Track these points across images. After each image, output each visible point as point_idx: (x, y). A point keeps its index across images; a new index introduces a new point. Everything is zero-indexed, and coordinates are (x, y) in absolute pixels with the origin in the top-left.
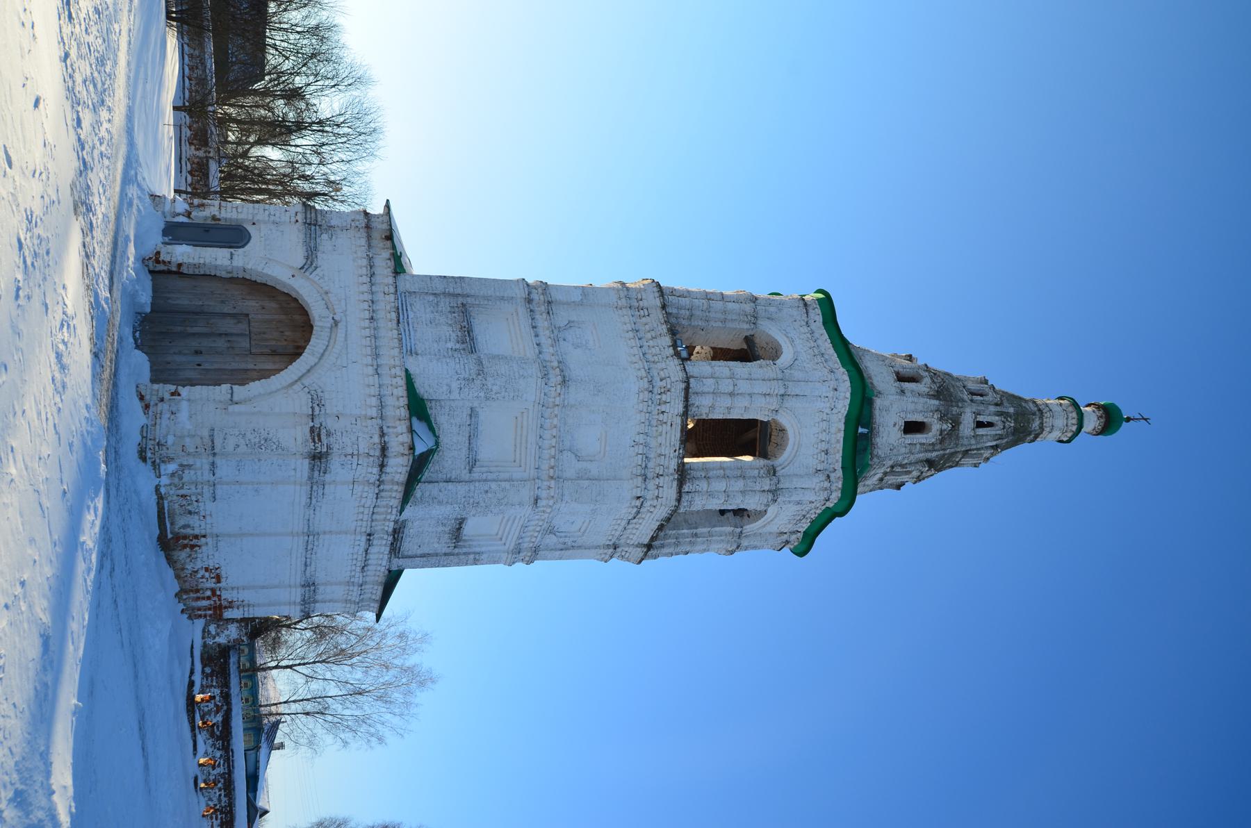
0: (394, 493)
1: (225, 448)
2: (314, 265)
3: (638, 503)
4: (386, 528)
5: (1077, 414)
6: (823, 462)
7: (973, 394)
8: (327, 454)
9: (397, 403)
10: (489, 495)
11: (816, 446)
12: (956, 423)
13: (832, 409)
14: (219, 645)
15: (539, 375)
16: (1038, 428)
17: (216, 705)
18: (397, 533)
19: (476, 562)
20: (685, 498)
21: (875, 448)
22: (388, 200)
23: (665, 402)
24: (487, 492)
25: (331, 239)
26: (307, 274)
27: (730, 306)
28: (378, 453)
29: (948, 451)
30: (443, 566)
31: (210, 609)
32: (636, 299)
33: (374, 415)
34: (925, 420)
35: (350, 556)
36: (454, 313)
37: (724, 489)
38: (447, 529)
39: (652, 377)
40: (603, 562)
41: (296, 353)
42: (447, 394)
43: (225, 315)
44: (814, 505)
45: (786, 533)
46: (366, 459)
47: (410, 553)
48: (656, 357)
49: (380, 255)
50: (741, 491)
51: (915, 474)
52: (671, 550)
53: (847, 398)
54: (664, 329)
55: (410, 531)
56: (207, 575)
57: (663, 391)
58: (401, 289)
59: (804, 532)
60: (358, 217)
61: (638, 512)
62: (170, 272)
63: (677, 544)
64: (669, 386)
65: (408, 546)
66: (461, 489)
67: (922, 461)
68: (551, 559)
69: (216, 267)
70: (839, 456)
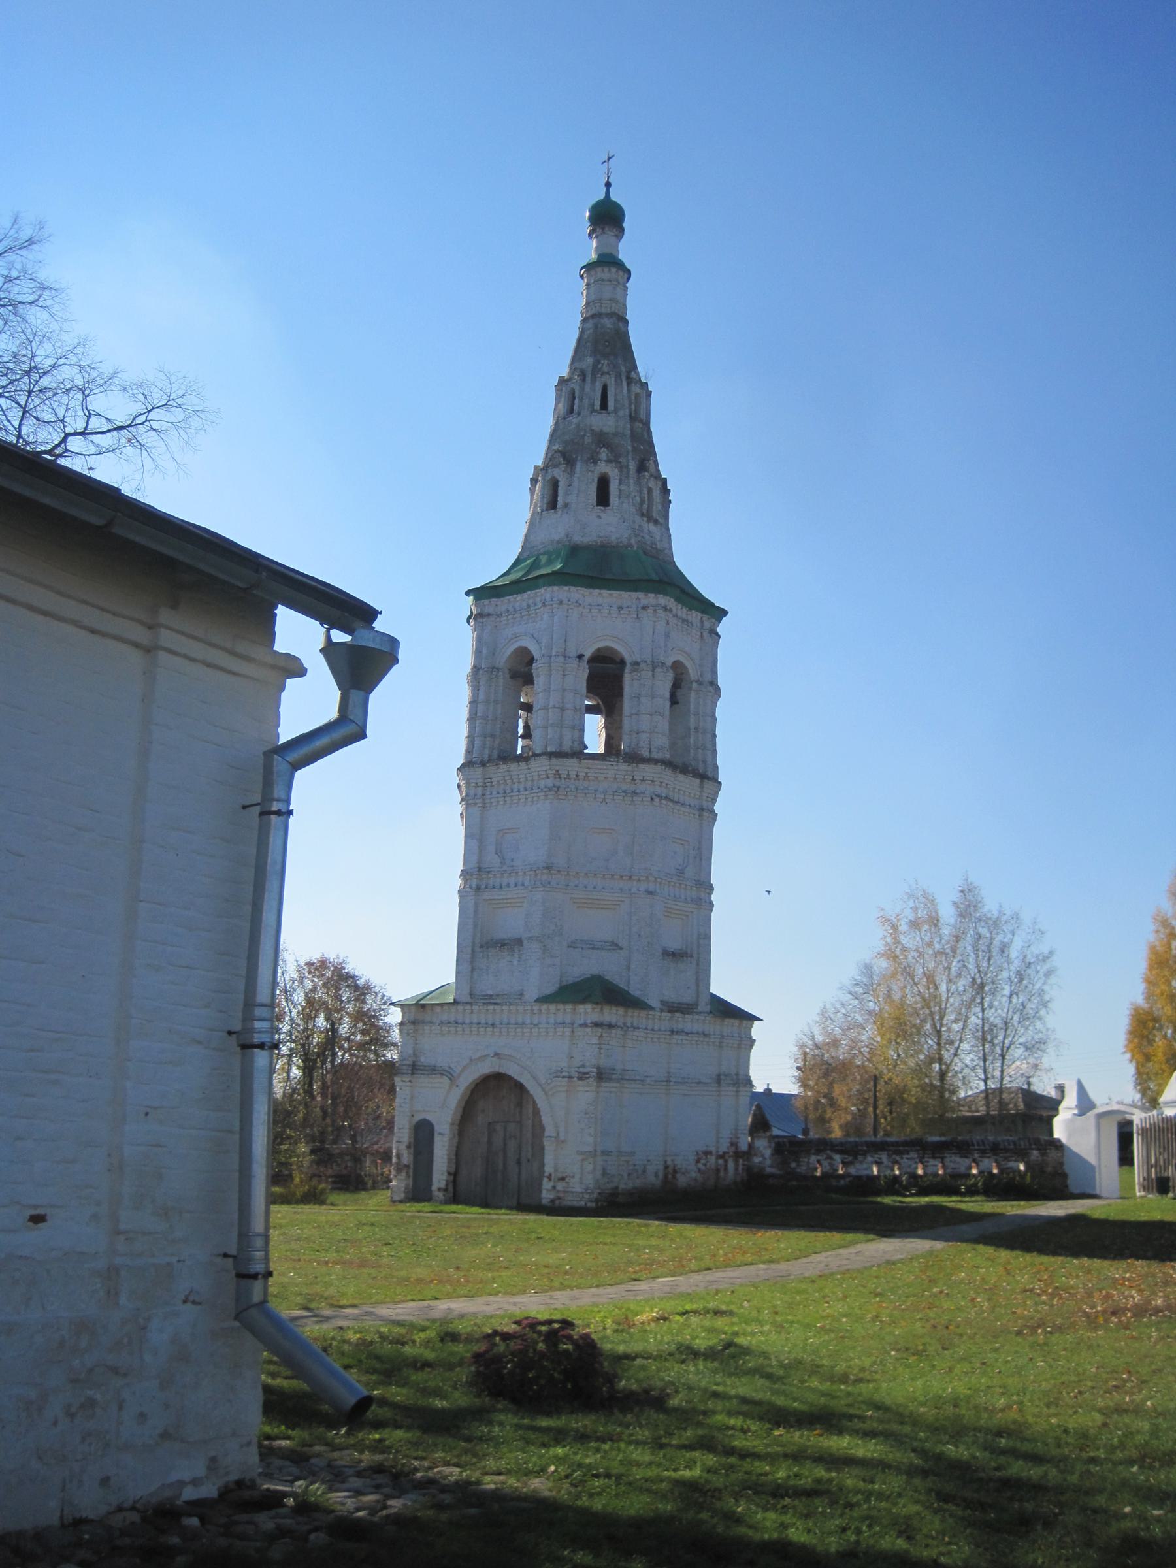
0: (635, 1017)
7: (571, 411)
8: (598, 1068)
12: (602, 440)
14: (772, 1155)
16: (611, 320)
18: (676, 1008)
23: (568, 775)
26: (455, 1075)
27: (482, 697)
28: (600, 1030)
33: (570, 1030)
41: (520, 1088)
43: (489, 1142)
52: (709, 753)
54: (503, 768)
55: (671, 996)
56: (702, 1162)
58: (468, 999)
61: (667, 798)
62: (454, 1182)
63: (704, 748)
65: (687, 997)
67: (639, 478)
70: (625, 594)
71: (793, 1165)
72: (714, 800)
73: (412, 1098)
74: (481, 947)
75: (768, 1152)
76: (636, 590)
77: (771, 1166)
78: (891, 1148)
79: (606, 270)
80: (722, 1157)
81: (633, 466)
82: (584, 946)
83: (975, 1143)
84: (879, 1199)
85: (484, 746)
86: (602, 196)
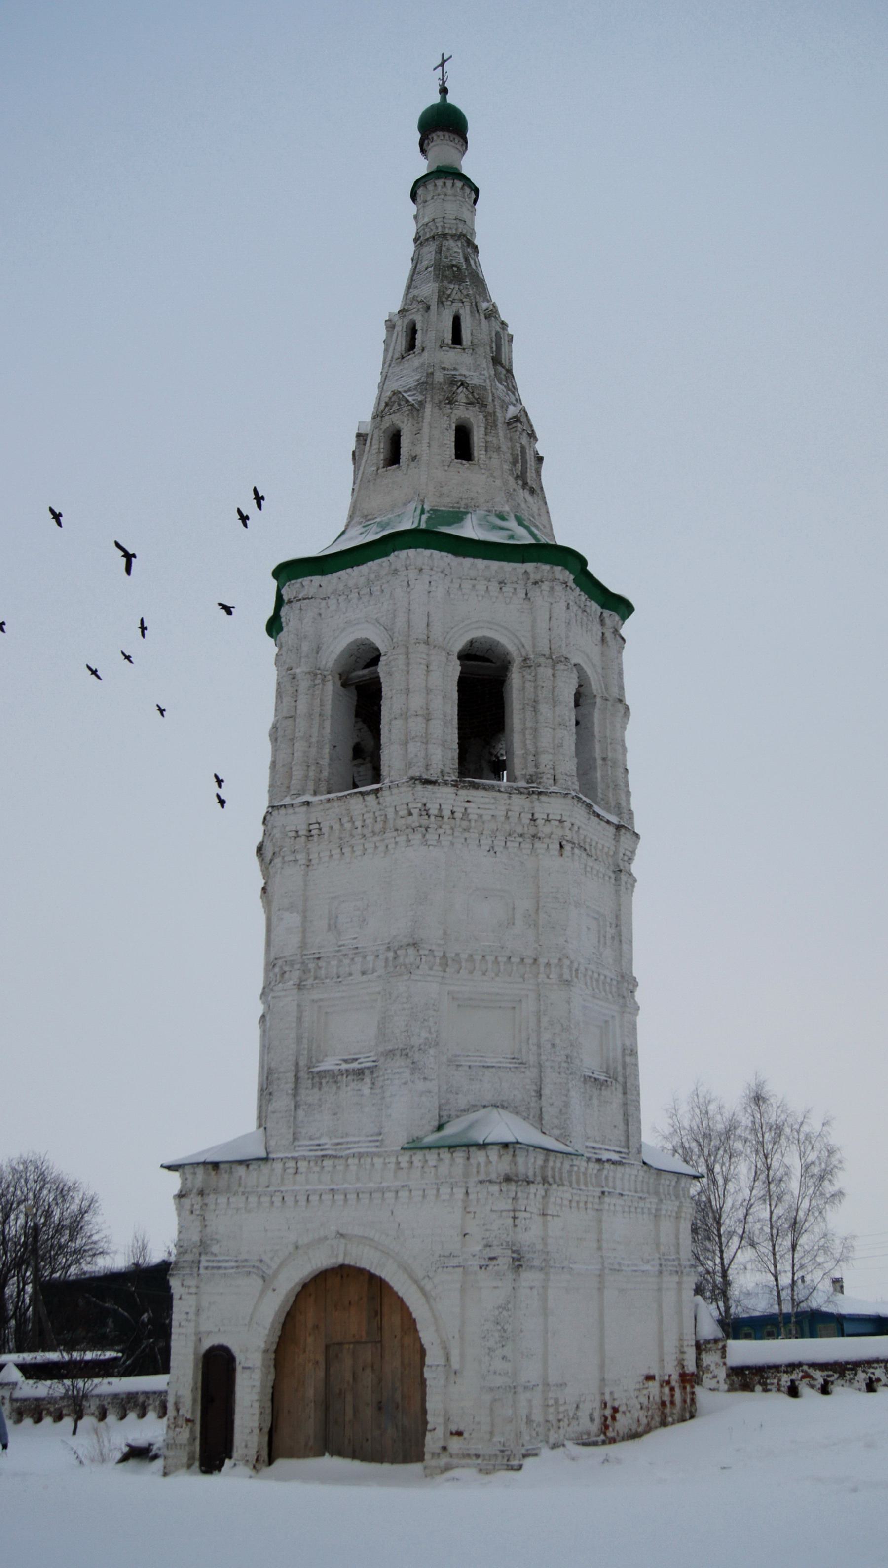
1: (508, 1373)
3: (568, 847)
4: (595, 1171)
5: (438, 178)
6: (515, 589)
9: (447, 1162)
10: (558, 1041)
11: (494, 599)
13: (446, 575)
15: (406, 977)
17: (803, 1377)
19: (633, 1053)
22: (162, 1166)
23: (440, 810)
24: (553, 1045)
25: (218, 1241)
28: (513, 1187)
30: (639, 1094)
31: (685, 1388)
32: (295, 837)
34: (454, 428)
35: (625, 1215)
36: (321, 1083)
37: (550, 730)
38: (596, 1093)
39: (407, 828)
40: (636, 884)
42: (432, 1097)
45: (603, 634)
46: (520, 1202)
47: (623, 1138)
48: (379, 819)
49: (240, 1177)
50: (554, 707)
51: (524, 440)
53: (431, 554)
57: (424, 813)
59: (603, 607)
60: (188, 1207)
64: (420, 805)
66: (550, 1078)
68: (631, 955)
69: (263, 1386)
73: (198, 1312)
80: (668, 1383)
84: (132, 1359)
86: (436, 99)
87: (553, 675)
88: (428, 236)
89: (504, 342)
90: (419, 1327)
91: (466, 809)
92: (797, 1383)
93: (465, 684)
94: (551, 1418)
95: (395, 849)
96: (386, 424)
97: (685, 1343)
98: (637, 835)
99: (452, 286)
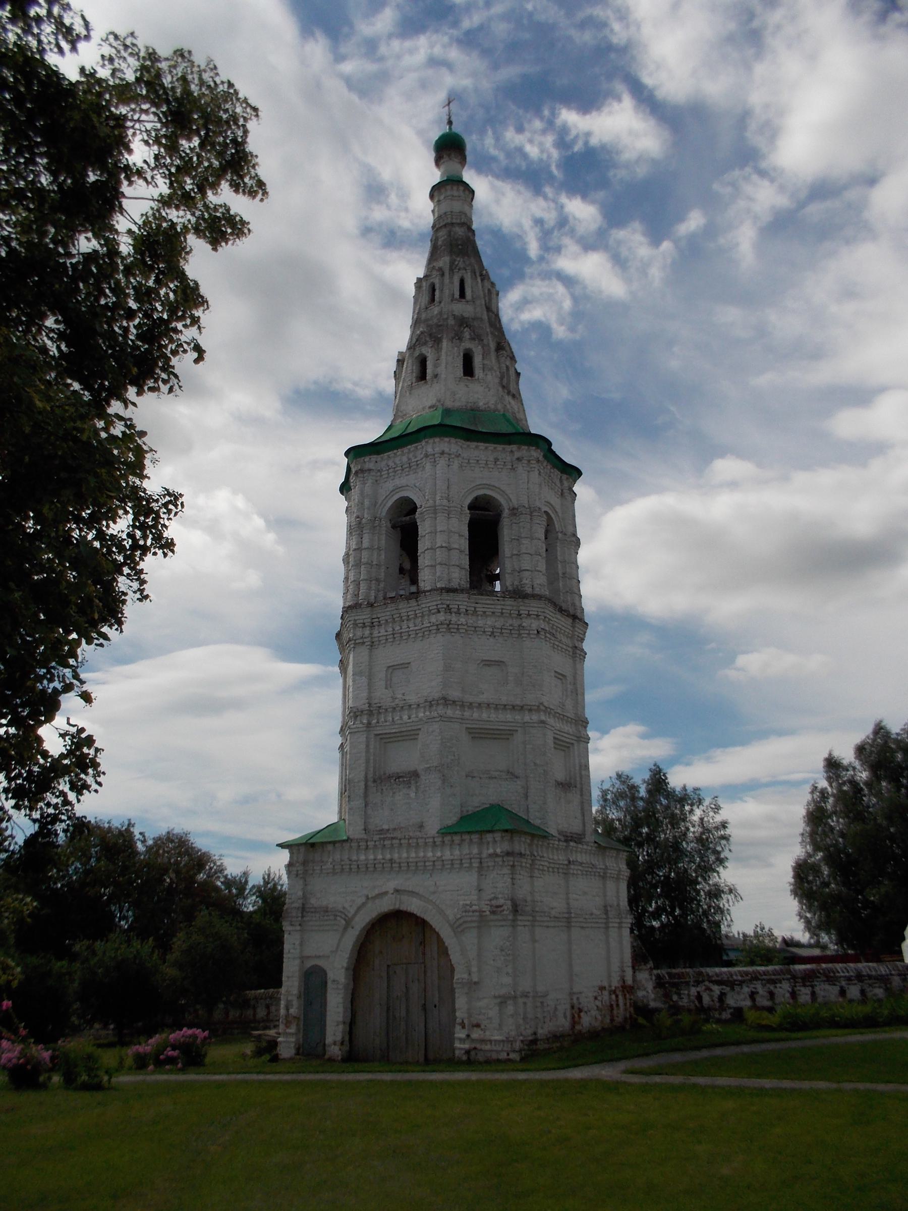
2: (342, 910)
12: (463, 322)
14: (655, 988)
16: (462, 230)
20: (537, 591)
21: (489, 407)
23: (459, 609)
27: (366, 544)
29: (488, 330)
31: (625, 995)
34: (462, 354)
41: (421, 924)
44: (542, 471)
59: (561, 473)
62: (351, 1033)
64: (445, 606)
71: (675, 998)
72: (582, 640)
74: (374, 781)
75: (650, 986)
76: (510, 444)
77: (655, 1000)
78: (764, 977)
79: (455, 188)
80: (614, 992)
81: (493, 346)
82: (482, 776)
83: (839, 970)
85: (369, 588)
87: (531, 519)
88: (441, 224)
89: (494, 296)
90: (450, 952)
91: (475, 608)
92: (701, 993)
93: (473, 525)
94: (539, 1015)
95: (429, 635)
96: (417, 353)
97: (625, 965)
98: (587, 624)
99: (458, 259)
